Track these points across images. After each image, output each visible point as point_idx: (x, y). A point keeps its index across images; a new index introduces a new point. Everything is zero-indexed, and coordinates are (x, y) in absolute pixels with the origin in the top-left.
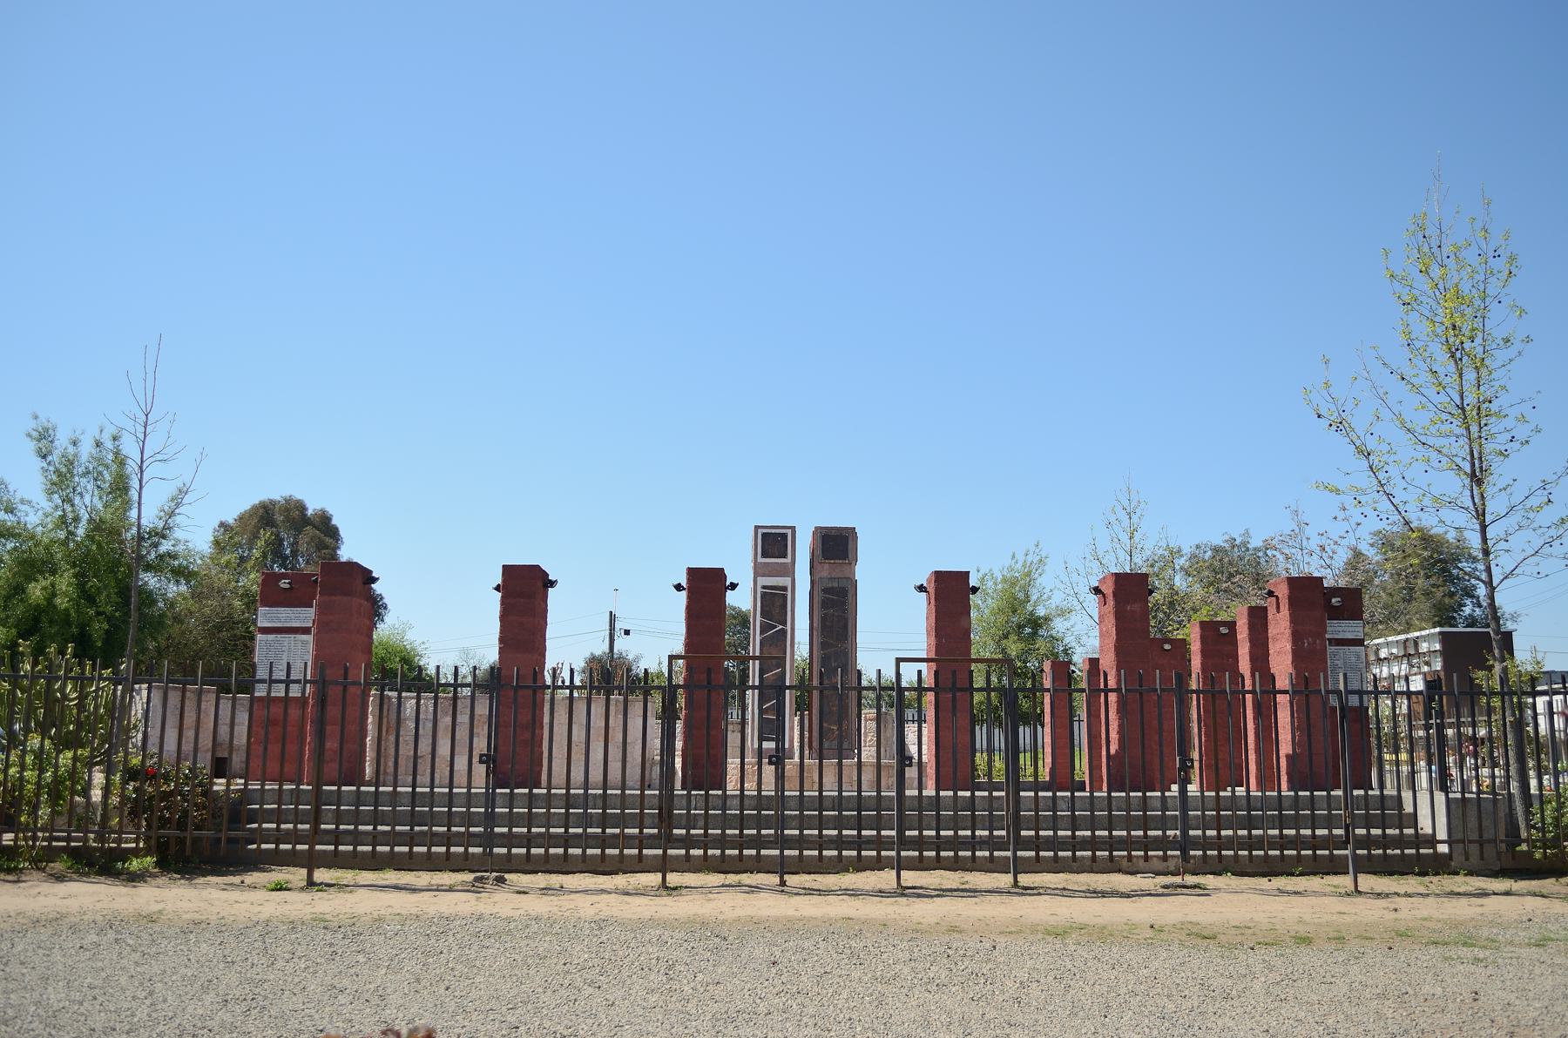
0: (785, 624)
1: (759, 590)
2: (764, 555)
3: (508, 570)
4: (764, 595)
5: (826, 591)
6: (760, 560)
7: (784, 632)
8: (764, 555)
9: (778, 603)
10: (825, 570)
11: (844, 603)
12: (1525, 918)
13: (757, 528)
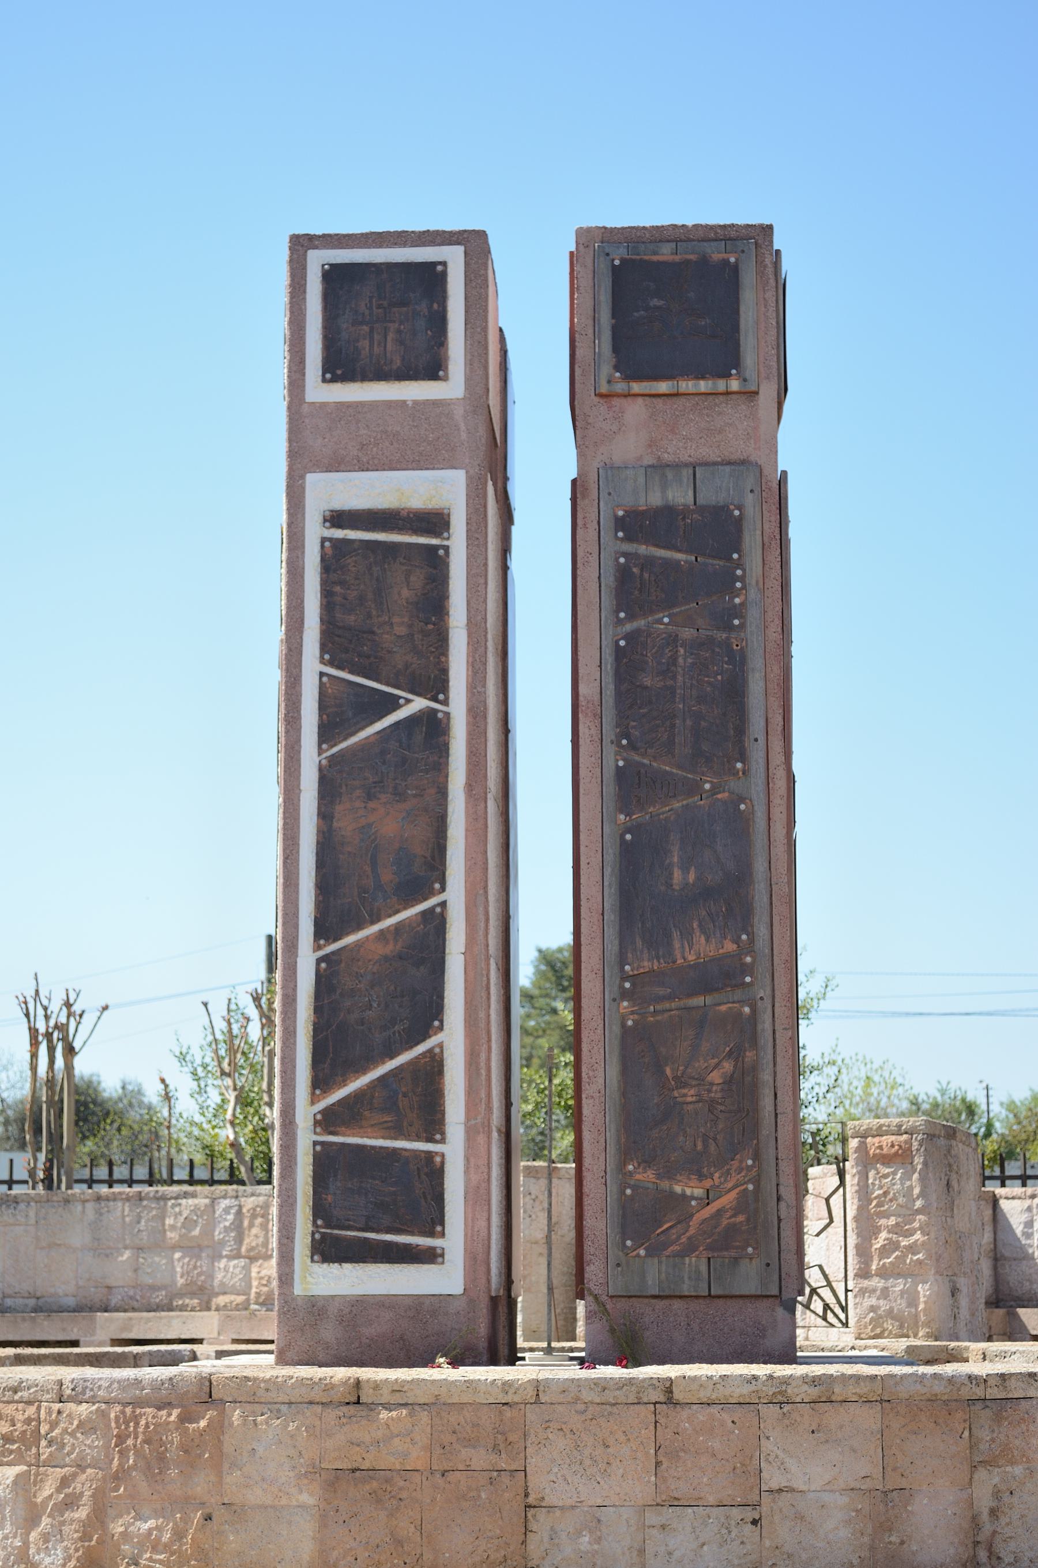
0: (436, 686)
1: (314, 532)
2: (339, 366)
3: (770, 227)
4: (335, 554)
5: (634, 525)
6: (320, 392)
7: (433, 729)
8: (339, 366)
9: (404, 590)
10: (636, 428)
11: (726, 582)
12: (561, 1433)
13: (301, 245)
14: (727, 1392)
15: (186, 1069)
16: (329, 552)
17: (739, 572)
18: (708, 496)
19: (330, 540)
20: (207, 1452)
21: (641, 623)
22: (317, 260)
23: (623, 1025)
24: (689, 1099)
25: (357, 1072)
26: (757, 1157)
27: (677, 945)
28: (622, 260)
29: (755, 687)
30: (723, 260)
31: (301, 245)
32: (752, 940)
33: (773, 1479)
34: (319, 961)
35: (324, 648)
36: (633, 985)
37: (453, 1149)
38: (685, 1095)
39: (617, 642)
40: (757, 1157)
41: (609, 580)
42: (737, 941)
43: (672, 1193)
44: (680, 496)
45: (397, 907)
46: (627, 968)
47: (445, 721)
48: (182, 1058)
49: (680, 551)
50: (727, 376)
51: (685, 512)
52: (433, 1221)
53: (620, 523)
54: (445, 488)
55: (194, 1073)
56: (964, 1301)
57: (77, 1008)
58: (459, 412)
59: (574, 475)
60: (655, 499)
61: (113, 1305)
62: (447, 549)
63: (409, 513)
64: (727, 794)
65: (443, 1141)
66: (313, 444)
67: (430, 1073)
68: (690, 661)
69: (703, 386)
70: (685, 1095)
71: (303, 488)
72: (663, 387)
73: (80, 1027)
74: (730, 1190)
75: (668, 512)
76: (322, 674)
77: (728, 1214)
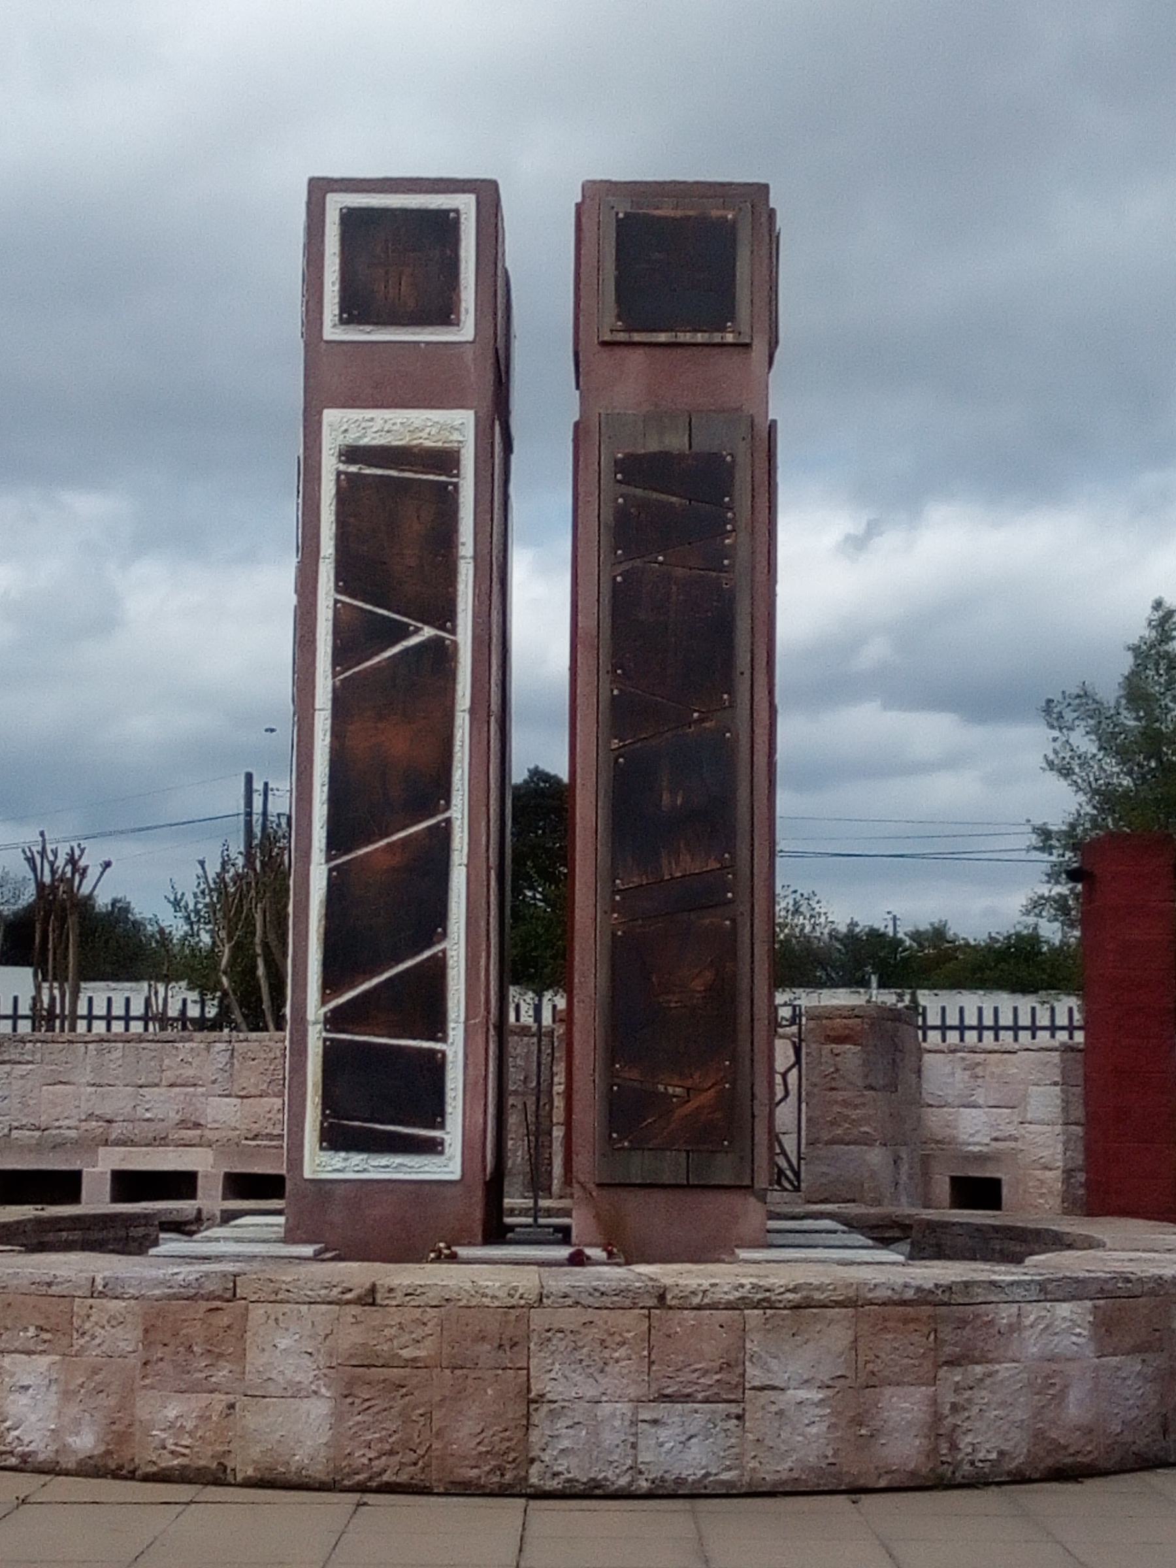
0: (445, 616)
1: (330, 465)
3: (766, 187)
5: (635, 469)
7: (440, 656)
13: (319, 188)
14: (717, 1297)
15: (179, 914)
16: (344, 484)
17: (730, 515)
18: (703, 444)
19: (346, 473)
20: (228, 1344)
21: (638, 563)
22: (336, 203)
23: (614, 934)
24: (673, 1005)
25: (364, 973)
26: (733, 1060)
27: (665, 862)
28: (626, 214)
29: (742, 625)
30: (722, 217)
31: (319, 188)
32: (733, 857)
33: (755, 1375)
34: (330, 871)
35: (338, 577)
36: (622, 899)
37: (454, 1048)
38: (670, 1001)
39: (614, 578)
40: (733, 1060)
41: (608, 515)
42: (720, 859)
43: (656, 1094)
44: (676, 442)
45: (407, 822)
46: (618, 881)
47: (451, 649)
48: (176, 904)
49: (674, 495)
50: (723, 329)
51: (681, 457)
52: (435, 1115)
53: (619, 465)
54: (454, 426)
55: (188, 918)
56: (904, 1168)
57: (82, 863)
58: (469, 356)
59: (577, 418)
60: (653, 446)
61: (113, 1137)
62: (456, 485)
63: (421, 450)
64: (713, 723)
65: (444, 1040)
66: (329, 380)
67: (434, 975)
68: (681, 597)
69: (700, 337)
70: (670, 1001)
71: (320, 423)
72: (662, 337)
73: (85, 882)
74: (709, 1088)
75: (664, 458)
76: (336, 601)
77: (706, 1111)
